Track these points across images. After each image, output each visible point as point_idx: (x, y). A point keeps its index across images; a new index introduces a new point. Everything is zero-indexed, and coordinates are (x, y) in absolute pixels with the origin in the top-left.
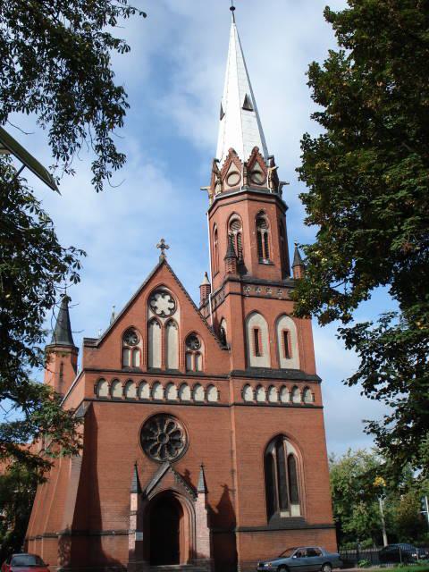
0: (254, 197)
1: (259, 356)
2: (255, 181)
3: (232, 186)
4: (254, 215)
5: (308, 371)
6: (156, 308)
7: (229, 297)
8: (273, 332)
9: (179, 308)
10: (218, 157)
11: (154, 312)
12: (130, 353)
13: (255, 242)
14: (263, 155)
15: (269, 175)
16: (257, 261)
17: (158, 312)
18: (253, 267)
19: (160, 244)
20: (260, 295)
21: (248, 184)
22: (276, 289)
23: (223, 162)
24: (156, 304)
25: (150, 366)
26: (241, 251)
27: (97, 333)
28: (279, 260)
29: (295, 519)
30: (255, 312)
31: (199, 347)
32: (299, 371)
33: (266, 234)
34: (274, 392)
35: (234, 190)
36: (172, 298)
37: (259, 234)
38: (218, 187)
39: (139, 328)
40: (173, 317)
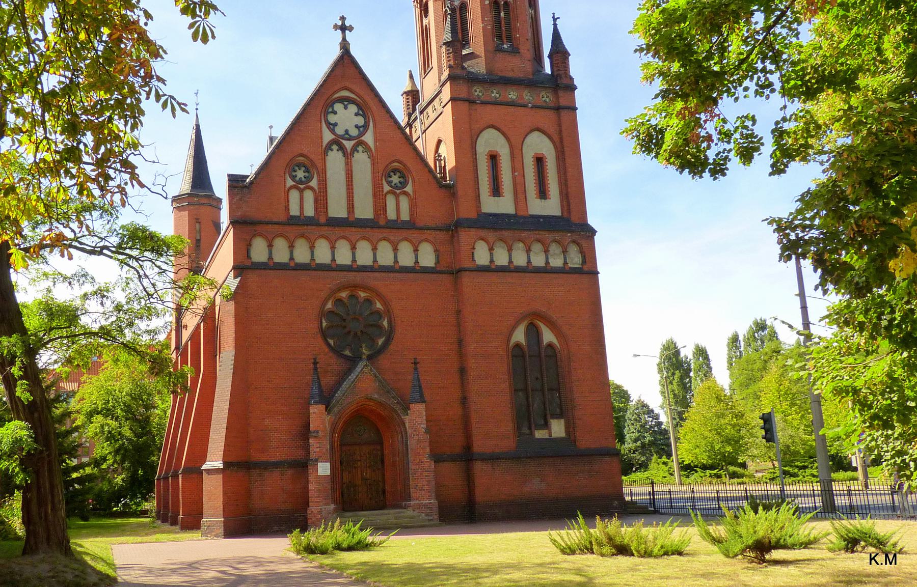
5: (521, 213)
17: (354, 132)
19: (340, 23)
27: (248, 167)
29: (559, 440)
32: (515, 216)
34: (280, 245)
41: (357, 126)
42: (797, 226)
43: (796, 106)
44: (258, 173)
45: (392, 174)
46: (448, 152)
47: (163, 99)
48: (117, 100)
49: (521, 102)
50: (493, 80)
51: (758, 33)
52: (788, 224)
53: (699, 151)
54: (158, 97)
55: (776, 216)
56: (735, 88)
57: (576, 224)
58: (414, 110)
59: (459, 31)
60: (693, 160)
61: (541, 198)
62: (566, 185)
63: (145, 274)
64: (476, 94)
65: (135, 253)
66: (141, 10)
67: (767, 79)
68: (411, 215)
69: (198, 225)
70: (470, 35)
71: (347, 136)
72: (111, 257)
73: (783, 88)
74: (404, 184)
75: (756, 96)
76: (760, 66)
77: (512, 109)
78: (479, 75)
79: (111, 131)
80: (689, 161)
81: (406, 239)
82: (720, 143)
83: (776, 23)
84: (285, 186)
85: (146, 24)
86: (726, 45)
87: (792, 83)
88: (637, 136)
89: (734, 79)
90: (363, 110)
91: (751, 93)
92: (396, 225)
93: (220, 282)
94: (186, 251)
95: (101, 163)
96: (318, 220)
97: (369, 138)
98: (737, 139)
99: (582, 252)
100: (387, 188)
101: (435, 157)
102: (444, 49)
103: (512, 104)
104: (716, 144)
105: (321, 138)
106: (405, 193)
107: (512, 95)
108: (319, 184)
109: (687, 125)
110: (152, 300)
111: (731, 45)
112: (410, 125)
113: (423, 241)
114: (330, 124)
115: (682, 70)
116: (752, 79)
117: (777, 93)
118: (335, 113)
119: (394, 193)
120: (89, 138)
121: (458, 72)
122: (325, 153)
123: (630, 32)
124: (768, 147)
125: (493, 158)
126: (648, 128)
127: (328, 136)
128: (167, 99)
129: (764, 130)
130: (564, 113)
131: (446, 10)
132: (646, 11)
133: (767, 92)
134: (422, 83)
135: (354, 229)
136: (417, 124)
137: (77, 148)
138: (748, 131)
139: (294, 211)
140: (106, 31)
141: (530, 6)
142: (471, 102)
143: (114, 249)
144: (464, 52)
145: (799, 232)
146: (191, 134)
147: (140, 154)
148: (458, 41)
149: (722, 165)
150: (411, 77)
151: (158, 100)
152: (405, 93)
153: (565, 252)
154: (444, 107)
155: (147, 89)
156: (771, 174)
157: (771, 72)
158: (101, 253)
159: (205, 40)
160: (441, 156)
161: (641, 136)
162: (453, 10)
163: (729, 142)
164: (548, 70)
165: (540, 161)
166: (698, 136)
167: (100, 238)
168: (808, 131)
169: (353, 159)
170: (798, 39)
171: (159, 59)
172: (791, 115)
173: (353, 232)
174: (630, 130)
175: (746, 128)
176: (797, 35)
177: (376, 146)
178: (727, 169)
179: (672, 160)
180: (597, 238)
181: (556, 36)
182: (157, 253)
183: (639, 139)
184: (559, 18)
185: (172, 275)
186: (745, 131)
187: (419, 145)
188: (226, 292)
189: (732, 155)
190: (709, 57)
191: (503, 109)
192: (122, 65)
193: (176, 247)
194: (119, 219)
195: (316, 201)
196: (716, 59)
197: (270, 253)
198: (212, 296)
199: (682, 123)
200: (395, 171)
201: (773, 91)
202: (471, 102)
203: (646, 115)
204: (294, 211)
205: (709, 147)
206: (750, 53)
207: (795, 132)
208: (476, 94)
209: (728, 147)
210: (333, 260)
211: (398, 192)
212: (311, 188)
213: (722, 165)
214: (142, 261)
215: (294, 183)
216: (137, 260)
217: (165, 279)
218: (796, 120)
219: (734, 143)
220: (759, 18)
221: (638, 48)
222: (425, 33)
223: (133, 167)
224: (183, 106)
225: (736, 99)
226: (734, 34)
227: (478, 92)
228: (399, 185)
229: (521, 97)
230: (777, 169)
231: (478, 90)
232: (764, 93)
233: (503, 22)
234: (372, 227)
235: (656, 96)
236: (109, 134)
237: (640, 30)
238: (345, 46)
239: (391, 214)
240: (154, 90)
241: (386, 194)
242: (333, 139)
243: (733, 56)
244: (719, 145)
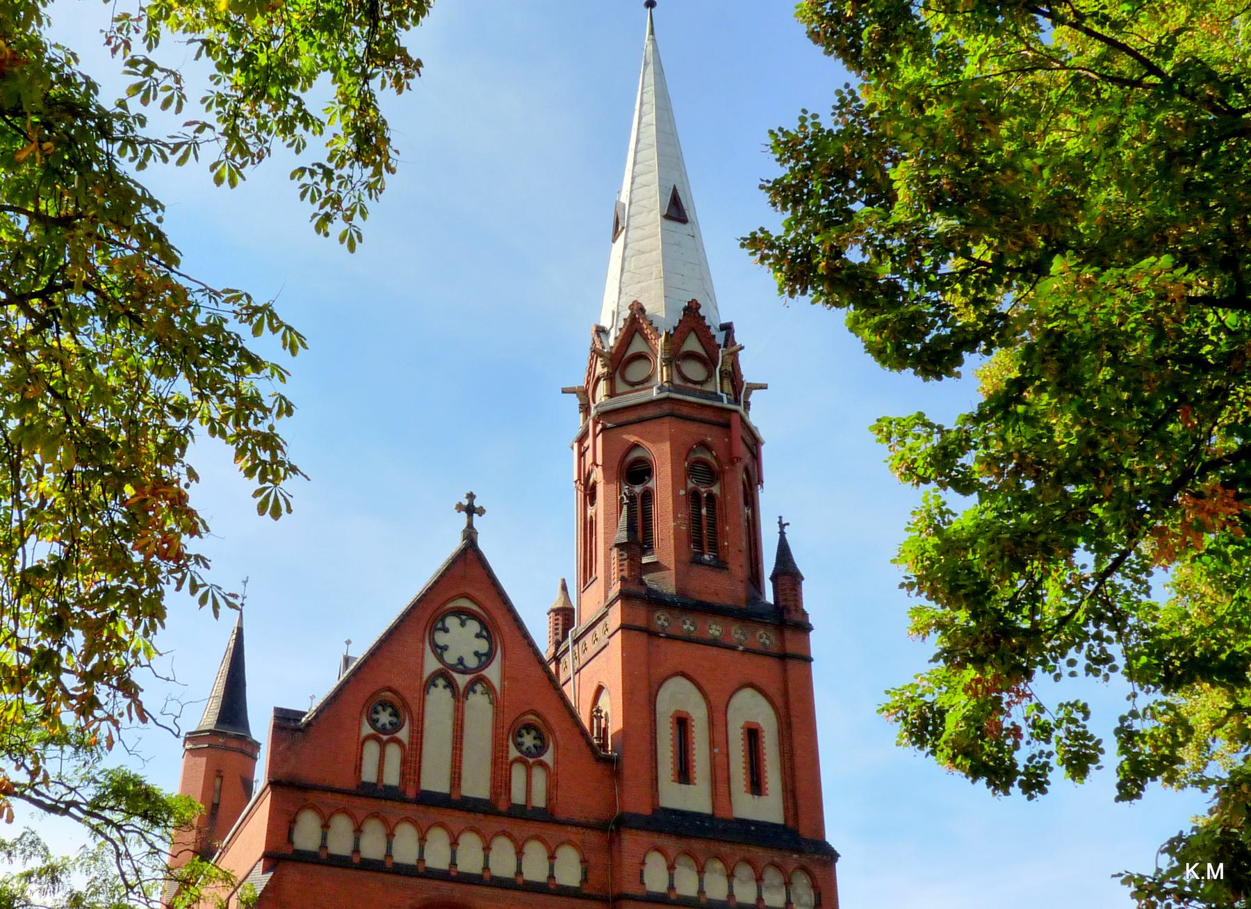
5: (721, 814)
10: (606, 322)
17: (472, 662)
19: (466, 502)
27: (307, 699)
32: (711, 817)
34: (342, 827)
41: (477, 654)
42: (1168, 892)
43: (1150, 697)
44: (320, 711)
45: (524, 732)
46: (612, 707)
47: (201, 591)
48: (129, 589)
49: (728, 641)
50: (685, 605)
51: (1086, 580)
52: (1155, 886)
53: (1001, 750)
54: (194, 588)
55: (1135, 871)
56: (1055, 660)
57: (805, 840)
58: (565, 636)
59: (640, 529)
60: (991, 763)
62: (793, 776)
63: (127, 850)
64: (659, 623)
65: (117, 817)
66: (183, 466)
67: (1103, 650)
68: (549, 799)
69: (218, 782)
70: (655, 536)
71: (460, 667)
72: (79, 819)
73: (1129, 666)
74: (541, 749)
75: (1087, 675)
76: (1091, 630)
77: (713, 651)
78: (666, 595)
79: (113, 634)
80: (985, 764)
81: (537, 838)
82: (1034, 742)
83: (1109, 572)
84: (359, 735)
85: (187, 486)
86: (1039, 592)
87: (1144, 659)
88: (904, 718)
89: (1052, 646)
90: (488, 630)
91: (1080, 668)
92: (523, 814)
93: (240, 879)
94: (195, 822)
95: (89, 678)
96: (404, 792)
97: (493, 673)
98: (1061, 738)
99: (815, 887)
100: (514, 753)
101: (592, 712)
102: (615, 553)
103: (714, 643)
104: (1028, 743)
105: (422, 667)
106: (543, 765)
107: (715, 630)
108: (411, 737)
109: (981, 707)
110: (131, 895)
111: (1046, 595)
112: (557, 659)
113: (562, 843)
114: (437, 646)
115: (972, 624)
116: (1080, 647)
117: (1119, 673)
118: (446, 630)
119: (525, 763)
120: (78, 640)
121: (634, 588)
122: (426, 689)
123: (894, 561)
124: (1112, 758)
125: (682, 723)
126: (920, 707)
127: (431, 664)
128: (208, 591)
129: (1102, 728)
130: (792, 665)
131: (622, 498)
132: (917, 533)
133: (1104, 669)
134: (579, 598)
135: (457, 813)
136: (568, 658)
137: (57, 654)
138: (1078, 727)
139: (369, 775)
140: (129, 490)
141: (746, 503)
142: (652, 634)
143: (85, 808)
144: (645, 560)
145: (1171, 901)
146: (228, 640)
147: (149, 666)
148: (637, 543)
149: (1040, 776)
150: (564, 588)
152: (553, 610)
153: (788, 884)
154: (609, 637)
155: (179, 575)
156: (1118, 799)
157: (1109, 640)
158: (65, 812)
160: (601, 711)
161: (909, 718)
162: (632, 498)
163: (1048, 741)
164: (769, 597)
165: (753, 735)
166: (999, 726)
167: (69, 788)
168: (1174, 736)
169: (468, 703)
170: (1149, 596)
171: (196, 537)
172: (1145, 710)
173: (456, 819)
174: (894, 708)
175: (1075, 721)
176: (1147, 592)
177: (502, 686)
178: (1048, 783)
179: (959, 760)
180: (839, 866)
181: (784, 551)
182: (151, 821)
183: (906, 723)
184: (788, 524)
185: (166, 859)
186: (1073, 728)
187: (569, 691)
188: (249, 894)
189: (1054, 761)
190: (1014, 605)
192: (145, 541)
193: (182, 815)
194: (102, 762)
195: (404, 762)
196: (1026, 612)
197: (324, 838)
198: (224, 898)
199: (973, 702)
200: (529, 727)
201: (1114, 669)
202: (652, 634)
203: (917, 687)
204: (369, 775)
205: (1016, 746)
206: (1076, 608)
207: (1152, 736)
208: (659, 623)
209: (1046, 748)
210: (421, 859)
211: (531, 760)
212: (398, 742)
213: (1040, 776)
214: (127, 832)
215: (372, 731)
216: (119, 828)
217: (156, 863)
218: (1154, 717)
219: (1058, 743)
220: (1084, 558)
221: (906, 582)
222: (588, 527)
223: (136, 689)
224: (231, 599)
225: (1058, 677)
226: (1050, 579)
227: (661, 620)
228: (533, 750)
229: (728, 634)
230: (1129, 788)
231: (663, 617)
232: (1099, 670)
233: (704, 523)
234: (485, 813)
235: (936, 659)
236: (108, 639)
237: (909, 559)
238: (470, 536)
239: (518, 796)
240: (188, 576)
241: (512, 763)
243: (1049, 613)
244: (1032, 745)
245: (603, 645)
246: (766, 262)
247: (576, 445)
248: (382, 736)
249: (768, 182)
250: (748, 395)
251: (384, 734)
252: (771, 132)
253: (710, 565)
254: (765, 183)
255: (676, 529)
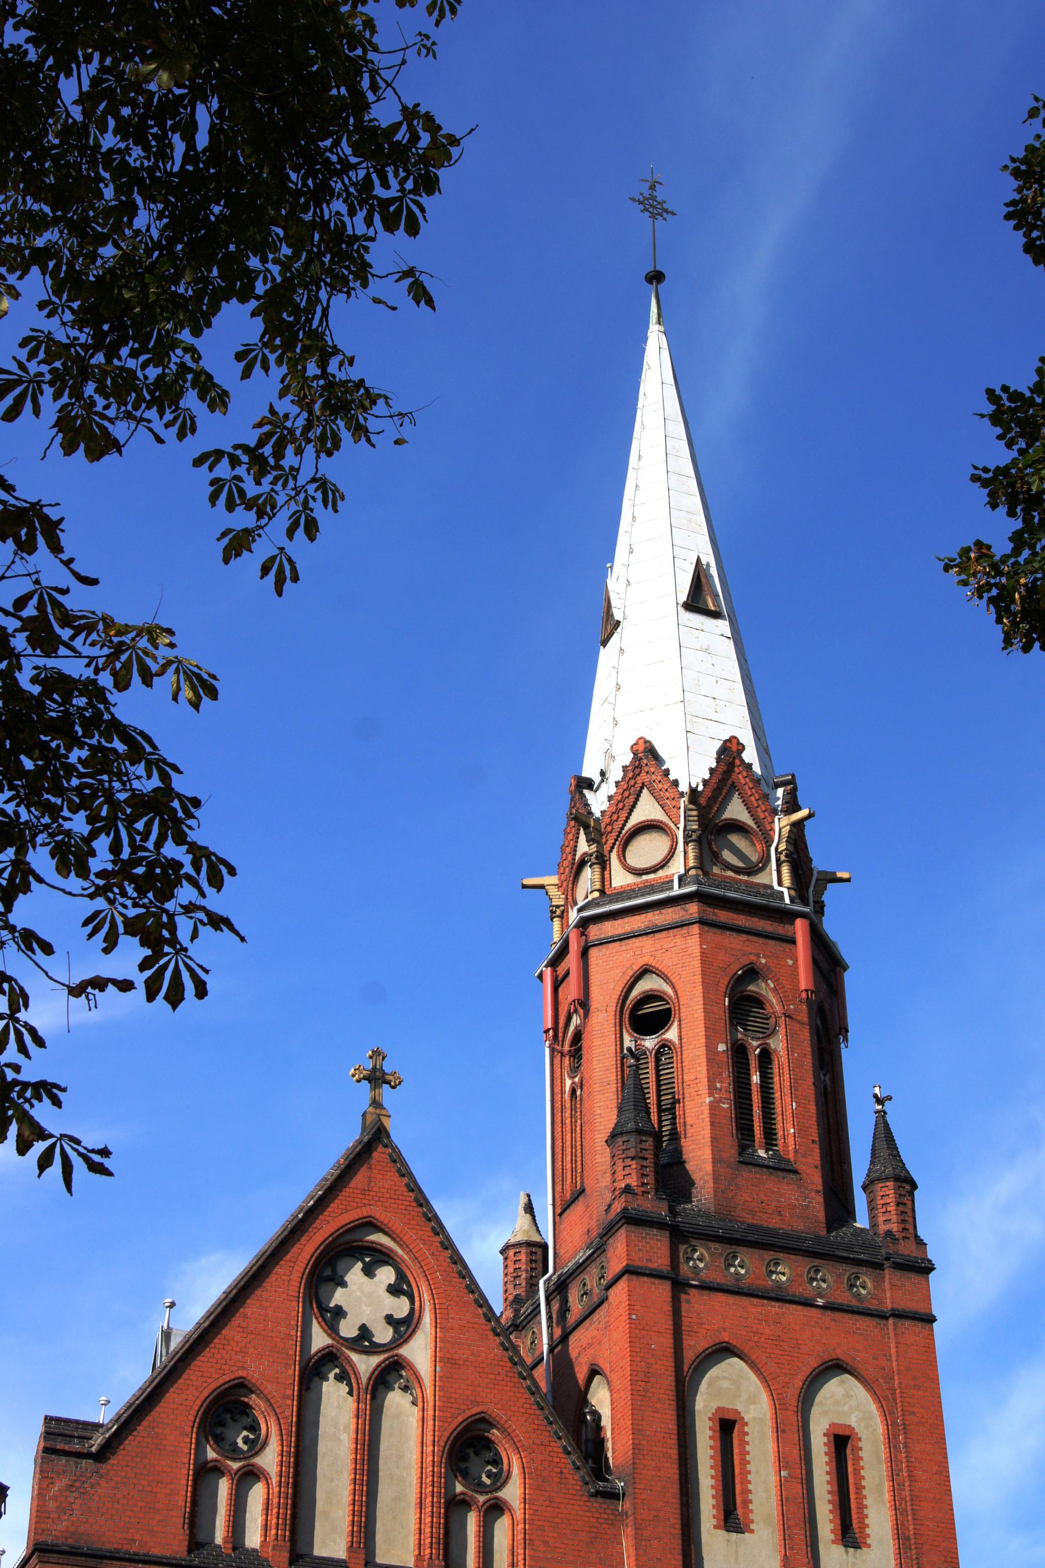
0: (724, 916)
1: (857, 1546)
2: (727, 855)
3: (638, 872)
4: (724, 982)
6: (339, 1313)
7: (622, 1285)
8: (794, 1436)
9: (427, 1318)
10: (590, 771)
11: (332, 1328)
12: (224, 1487)
13: (725, 1084)
14: (757, 769)
15: (779, 844)
16: (731, 1152)
17: (348, 1329)
18: (716, 1177)
20: (744, 1283)
21: (701, 866)
22: (804, 1265)
23: (609, 789)
24: (339, 1297)
25: (302, 1550)
26: (670, 1108)
28: (815, 1156)
30: (723, 1351)
31: (500, 1480)
33: (766, 1057)
35: (651, 888)
36: (401, 1276)
37: (739, 1051)
38: (589, 876)
39: (269, 1388)
40: (404, 1351)
41: (390, 1319)
61: (728, 1529)
77: (775, 1308)
103: (778, 1296)
151: (23, 1148)
159: (175, 998)
191: (754, 1308)
242: (328, 1347)
245: (596, 1300)
246: (985, 595)
247: (548, 972)
248: (229, 1463)
249: (986, 470)
250: (820, 891)
251: (234, 1459)
252: (990, 392)
253: (768, 1167)
254: (980, 473)
255: (713, 1107)
